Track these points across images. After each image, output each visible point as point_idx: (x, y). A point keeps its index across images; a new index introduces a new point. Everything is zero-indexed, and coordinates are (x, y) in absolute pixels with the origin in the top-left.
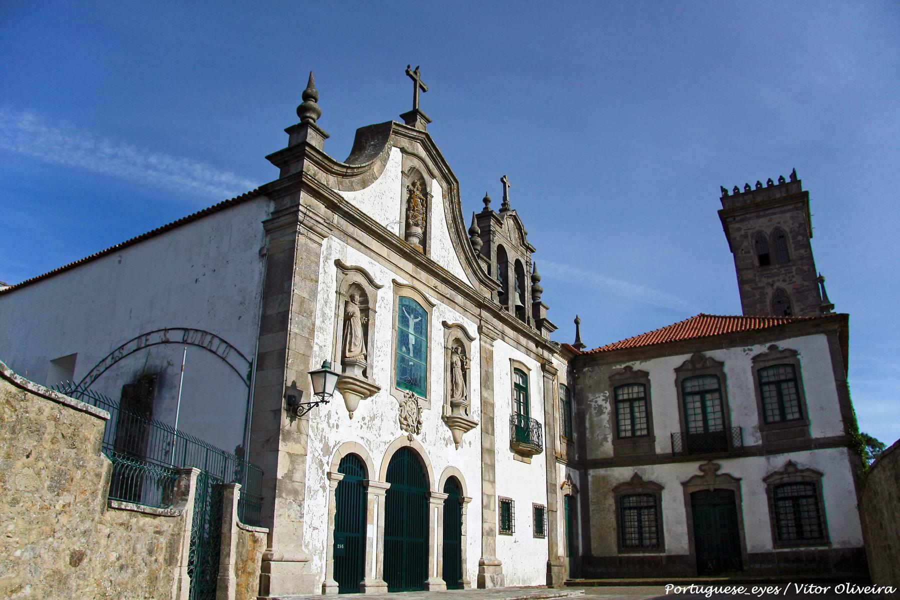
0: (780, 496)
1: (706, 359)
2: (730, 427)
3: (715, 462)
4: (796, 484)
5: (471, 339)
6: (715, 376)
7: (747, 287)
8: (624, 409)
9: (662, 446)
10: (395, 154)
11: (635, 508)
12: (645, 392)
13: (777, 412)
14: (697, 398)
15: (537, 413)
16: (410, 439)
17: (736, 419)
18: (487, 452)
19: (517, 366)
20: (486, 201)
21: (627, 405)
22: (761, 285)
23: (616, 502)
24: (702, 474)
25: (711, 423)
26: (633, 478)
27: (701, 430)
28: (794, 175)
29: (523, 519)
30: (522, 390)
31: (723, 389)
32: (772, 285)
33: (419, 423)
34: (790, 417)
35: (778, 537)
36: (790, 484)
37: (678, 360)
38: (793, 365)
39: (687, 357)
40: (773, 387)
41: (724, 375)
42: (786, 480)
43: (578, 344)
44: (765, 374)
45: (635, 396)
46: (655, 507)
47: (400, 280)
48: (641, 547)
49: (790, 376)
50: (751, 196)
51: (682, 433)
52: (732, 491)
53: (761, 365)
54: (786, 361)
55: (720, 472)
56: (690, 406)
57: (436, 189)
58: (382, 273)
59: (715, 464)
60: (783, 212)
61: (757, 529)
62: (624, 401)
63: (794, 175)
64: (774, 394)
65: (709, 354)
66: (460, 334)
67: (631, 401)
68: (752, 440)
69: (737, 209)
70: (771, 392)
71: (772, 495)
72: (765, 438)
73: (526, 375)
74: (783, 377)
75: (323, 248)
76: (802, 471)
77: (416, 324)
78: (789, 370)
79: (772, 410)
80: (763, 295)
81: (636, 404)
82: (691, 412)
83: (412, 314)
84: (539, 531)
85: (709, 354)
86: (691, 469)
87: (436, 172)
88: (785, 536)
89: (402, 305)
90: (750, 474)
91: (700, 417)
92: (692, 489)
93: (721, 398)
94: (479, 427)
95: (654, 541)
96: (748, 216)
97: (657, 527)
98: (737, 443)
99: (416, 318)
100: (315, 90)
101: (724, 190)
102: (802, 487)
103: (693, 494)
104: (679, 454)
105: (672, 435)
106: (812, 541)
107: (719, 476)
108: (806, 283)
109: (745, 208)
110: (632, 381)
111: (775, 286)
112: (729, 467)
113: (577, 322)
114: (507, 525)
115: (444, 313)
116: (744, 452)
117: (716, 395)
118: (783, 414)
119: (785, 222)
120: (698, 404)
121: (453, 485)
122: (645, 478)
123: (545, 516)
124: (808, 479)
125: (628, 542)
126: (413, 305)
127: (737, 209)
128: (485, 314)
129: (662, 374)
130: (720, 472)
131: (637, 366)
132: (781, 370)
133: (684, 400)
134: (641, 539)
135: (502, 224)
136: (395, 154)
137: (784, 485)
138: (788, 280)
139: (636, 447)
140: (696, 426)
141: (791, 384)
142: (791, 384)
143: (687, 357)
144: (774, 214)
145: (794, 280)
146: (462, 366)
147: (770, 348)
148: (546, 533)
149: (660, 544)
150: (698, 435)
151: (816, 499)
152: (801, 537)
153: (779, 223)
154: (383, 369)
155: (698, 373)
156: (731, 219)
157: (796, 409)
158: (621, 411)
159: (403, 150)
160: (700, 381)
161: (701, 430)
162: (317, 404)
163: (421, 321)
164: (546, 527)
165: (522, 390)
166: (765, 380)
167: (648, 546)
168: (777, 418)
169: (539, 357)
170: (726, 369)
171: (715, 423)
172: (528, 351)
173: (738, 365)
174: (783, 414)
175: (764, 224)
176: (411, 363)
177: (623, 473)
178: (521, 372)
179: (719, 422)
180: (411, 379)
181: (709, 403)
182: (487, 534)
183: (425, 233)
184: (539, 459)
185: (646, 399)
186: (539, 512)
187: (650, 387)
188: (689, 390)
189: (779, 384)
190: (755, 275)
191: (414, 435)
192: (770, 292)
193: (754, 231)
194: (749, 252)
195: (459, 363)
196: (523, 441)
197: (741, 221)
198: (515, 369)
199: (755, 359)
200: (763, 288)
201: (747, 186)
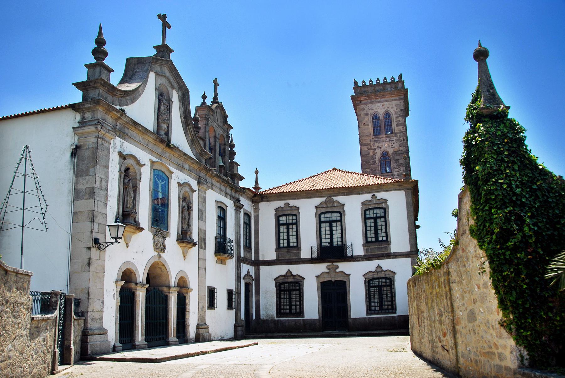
0: (372, 285)
3: (335, 264)
4: (381, 278)
5: (194, 191)
6: (339, 212)
7: (365, 148)
8: (283, 229)
9: (305, 254)
10: (152, 76)
11: (287, 290)
12: (296, 219)
13: (373, 236)
14: (328, 224)
15: (230, 234)
16: (160, 257)
17: (349, 240)
18: (201, 260)
19: (220, 205)
20: (204, 97)
21: (285, 227)
22: (373, 147)
23: (276, 286)
24: (328, 271)
26: (287, 273)
28: (400, 77)
29: (221, 299)
30: (222, 219)
31: (343, 221)
32: (380, 148)
33: (164, 246)
34: (380, 239)
35: (369, 310)
36: (378, 278)
37: (318, 201)
38: (384, 209)
39: (323, 199)
41: (344, 212)
42: (375, 276)
43: (257, 187)
45: (291, 221)
46: (341, 221)
47: (155, 159)
48: (290, 314)
49: (382, 215)
50: (372, 88)
51: (317, 246)
52: (345, 282)
53: (365, 208)
55: (337, 270)
57: (175, 96)
58: (144, 157)
60: (392, 101)
61: (358, 305)
62: (283, 224)
63: (400, 77)
64: (373, 225)
65: (335, 198)
66: (187, 189)
68: (359, 251)
69: (362, 94)
70: (371, 223)
71: (367, 285)
72: (366, 251)
75: (111, 145)
76: (385, 271)
77: (162, 185)
78: (382, 211)
80: (374, 154)
81: (291, 227)
82: (323, 233)
83: (161, 179)
84: (230, 306)
85: (335, 198)
86: (322, 268)
87: (175, 85)
88: (373, 308)
89: (155, 175)
90: (356, 274)
92: (322, 280)
93: (341, 226)
94: (197, 246)
95: (298, 310)
97: (300, 302)
98: (349, 253)
99: (162, 181)
100: (105, 36)
101: (356, 83)
102: (384, 280)
103: (322, 283)
106: (387, 311)
108: (401, 149)
110: (289, 212)
111: (382, 149)
112: (343, 267)
113: (257, 172)
114: (212, 305)
115: (178, 177)
116: (353, 259)
118: (377, 236)
119: (392, 108)
120: (328, 229)
121: (183, 285)
122: (294, 273)
123: (234, 296)
124: (388, 276)
125: (282, 311)
126: (161, 174)
127: (362, 94)
129: (308, 211)
130: (337, 270)
131: (292, 203)
132: (378, 211)
133: (320, 228)
134: (290, 309)
136: (152, 76)
137: (374, 279)
138: (390, 145)
139: (288, 253)
141: (383, 220)
142: (383, 220)
143: (323, 199)
144: (386, 101)
145: (394, 145)
146: (188, 209)
148: (234, 307)
149: (301, 313)
151: (391, 287)
152: (382, 310)
153: (388, 108)
154: (144, 215)
155: (329, 210)
156: (359, 102)
157: (384, 235)
159: (156, 73)
160: (330, 216)
162: (112, 243)
163: (165, 183)
164: (234, 303)
165: (222, 219)
167: (294, 314)
169: (232, 198)
170: (345, 208)
171: (337, 242)
172: (226, 194)
173: (353, 207)
174: (377, 236)
175: (379, 108)
176: (160, 210)
177: (281, 270)
178: (222, 209)
179: (339, 240)
180: (159, 218)
181: (334, 228)
182: (201, 311)
183: (168, 127)
184: (231, 263)
185: (297, 224)
186: (230, 293)
188: (323, 220)
189: (376, 217)
190: (371, 141)
191: (162, 254)
192: (379, 153)
193: (372, 111)
194: (368, 125)
195: (186, 207)
196: (222, 248)
197: (366, 104)
198: (219, 207)
199: (363, 203)
200: (375, 149)
201: (371, 80)
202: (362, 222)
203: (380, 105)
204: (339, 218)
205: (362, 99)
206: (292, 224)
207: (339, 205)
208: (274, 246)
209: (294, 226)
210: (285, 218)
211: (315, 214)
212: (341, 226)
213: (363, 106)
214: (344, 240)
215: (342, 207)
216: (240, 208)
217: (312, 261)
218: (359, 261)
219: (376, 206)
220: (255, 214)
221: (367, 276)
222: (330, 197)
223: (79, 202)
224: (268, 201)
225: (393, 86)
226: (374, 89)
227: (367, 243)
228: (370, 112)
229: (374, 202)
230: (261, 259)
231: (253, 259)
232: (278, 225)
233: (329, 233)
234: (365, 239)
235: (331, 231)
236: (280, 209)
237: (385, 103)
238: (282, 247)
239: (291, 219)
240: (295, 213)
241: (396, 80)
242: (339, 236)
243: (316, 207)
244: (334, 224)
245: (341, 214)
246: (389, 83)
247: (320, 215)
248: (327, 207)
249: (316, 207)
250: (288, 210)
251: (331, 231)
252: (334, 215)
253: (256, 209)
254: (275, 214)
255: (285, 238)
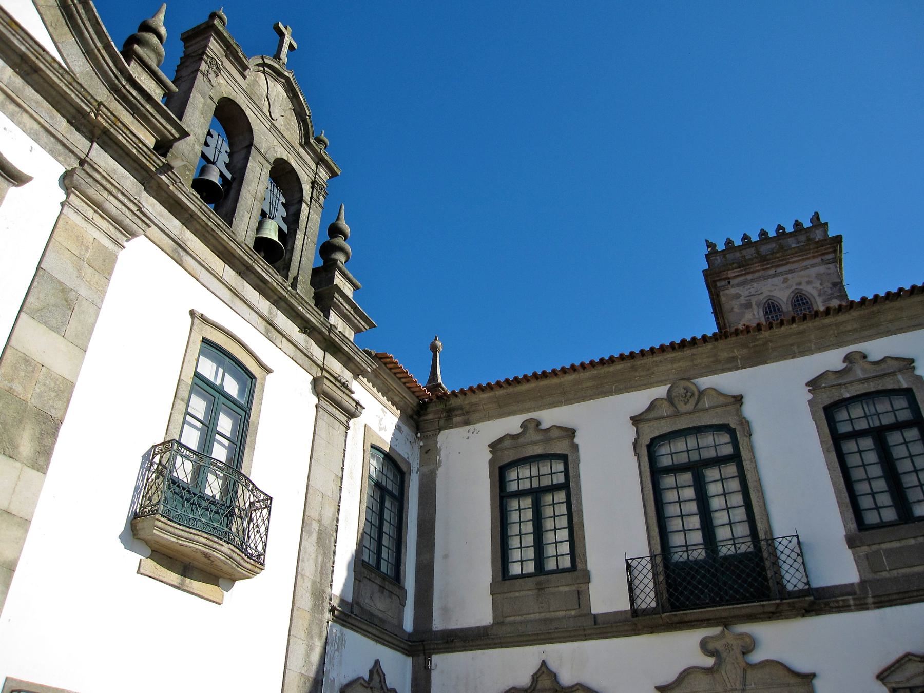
1: (702, 393)
2: (771, 540)
8: (520, 511)
9: (607, 595)
12: (566, 472)
13: (885, 499)
14: (687, 478)
24: (709, 662)
25: (723, 533)
26: (535, 678)
27: (699, 554)
31: (745, 454)
40: (867, 443)
41: (746, 425)
44: (842, 415)
45: (546, 482)
46: (736, 458)
50: (753, 250)
51: (653, 557)
53: (826, 398)
54: (889, 384)
55: (757, 657)
56: (671, 496)
59: (742, 636)
60: (806, 268)
62: (519, 494)
64: (872, 457)
65: (705, 382)
67: (536, 494)
68: (839, 567)
72: (867, 563)
73: (252, 377)
74: (887, 420)
79: (873, 494)
82: (672, 510)
91: (695, 522)
93: (742, 476)
96: (749, 277)
98: (793, 580)
101: (710, 245)
104: (646, 612)
105: (629, 566)
107: (753, 666)
109: (744, 265)
110: (538, 450)
112: (780, 640)
116: (819, 601)
117: (731, 469)
119: (809, 283)
122: (567, 678)
128: (102, 158)
130: (757, 657)
131: (550, 417)
132: (883, 406)
135: (245, 68)
140: (688, 539)
144: (791, 272)
147: (848, 358)
150: (690, 565)
153: (800, 284)
156: (723, 283)
158: (514, 517)
161: (699, 554)
166: (844, 428)
168: (890, 515)
170: (749, 410)
171: (731, 535)
179: (742, 530)
181: (714, 489)
185: (568, 487)
187: (577, 461)
188: (666, 461)
193: (761, 297)
197: (738, 285)
199: (814, 385)
202: (826, 451)
203: (777, 280)
204: (728, 450)
205: (731, 274)
206: (553, 488)
207: (721, 400)
208: (485, 573)
209: (561, 496)
210: (525, 472)
211: (635, 445)
212: (742, 476)
213: (733, 291)
214: (760, 526)
215: (732, 408)
216: (351, 415)
217: (635, 622)
218: (843, 608)
219: (872, 387)
220: (425, 469)
221: (898, 678)
222: (688, 379)
223: (9, 555)
224: (467, 423)
225: (803, 238)
226: (758, 252)
227: (861, 530)
228: (754, 300)
229: (860, 374)
230: (438, 624)
231: (408, 625)
232: (502, 496)
233: (693, 507)
234: (850, 514)
235: (702, 499)
236: (507, 443)
237: (789, 276)
238: (516, 577)
239: (554, 472)
240: (562, 450)
241: (807, 224)
242: (740, 514)
243: (636, 420)
244: (712, 474)
245: (732, 432)
246: (791, 234)
247: (652, 447)
248: (677, 414)
249: (636, 420)
250: (533, 443)
251: (702, 499)
252: (708, 440)
253: (429, 453)
254: (491, 462)
255: (529, 540)
